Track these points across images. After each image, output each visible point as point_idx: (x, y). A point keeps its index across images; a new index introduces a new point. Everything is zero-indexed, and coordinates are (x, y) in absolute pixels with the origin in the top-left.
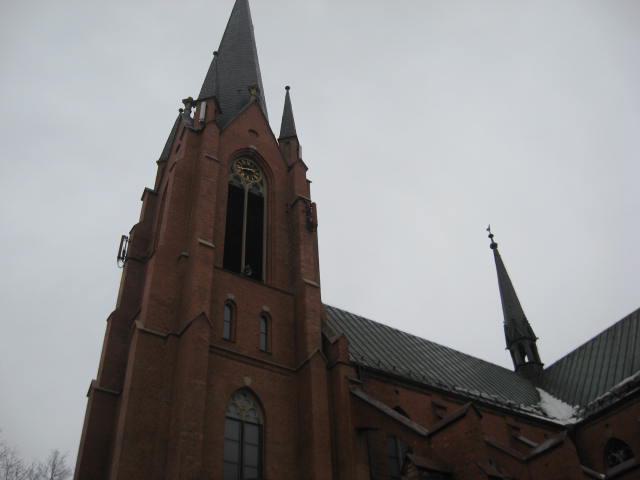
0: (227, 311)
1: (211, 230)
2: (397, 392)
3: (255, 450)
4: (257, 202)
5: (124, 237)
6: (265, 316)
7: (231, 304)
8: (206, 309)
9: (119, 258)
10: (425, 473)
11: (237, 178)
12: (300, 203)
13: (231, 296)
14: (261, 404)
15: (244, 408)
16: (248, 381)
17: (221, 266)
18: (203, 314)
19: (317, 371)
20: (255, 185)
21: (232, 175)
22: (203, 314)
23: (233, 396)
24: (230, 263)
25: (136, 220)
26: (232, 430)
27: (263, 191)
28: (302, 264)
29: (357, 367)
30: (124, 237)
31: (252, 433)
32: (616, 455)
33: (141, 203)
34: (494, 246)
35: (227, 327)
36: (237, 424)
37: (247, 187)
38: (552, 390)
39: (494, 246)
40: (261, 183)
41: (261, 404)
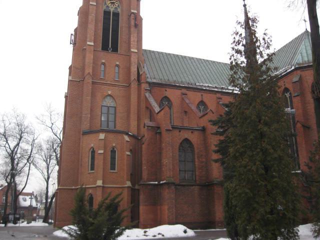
0: (103, 66)
1: (93, 37)
2: (166, 90)
3: (113, 116)
4: (116, 15)
5: (72, 34)
6: (117, 66)
7: (104, 64)
8: (91, 71)
9: (71, 43)
10: (150, 128)
11: (108, 7)
12: (132, 15)
13: (103, 61)
14: (114, 99)
15: (109, 102)
16: (110, 92)
17: (100, 49)
18: (89, 73)
19: (134, 85)
20: (116, 8)
21: (105, 6)
22: (89, 73)
23: (104, 98)
24: (105, 48)
25: (76, 25)
26: (105, 110)
27: (119, 10)
28: (132, 43)
29: (150, 84)
30: (72, 34)
31: (112, 111)
32: (286, 94)
33: (77, 17)
34: (245, 6)
35: (102, 73)
36: (106, 108)
37: (112, 10)
38: (194, 98)
39: (245, 6)
40: (119, 6)
41: (114, 99)
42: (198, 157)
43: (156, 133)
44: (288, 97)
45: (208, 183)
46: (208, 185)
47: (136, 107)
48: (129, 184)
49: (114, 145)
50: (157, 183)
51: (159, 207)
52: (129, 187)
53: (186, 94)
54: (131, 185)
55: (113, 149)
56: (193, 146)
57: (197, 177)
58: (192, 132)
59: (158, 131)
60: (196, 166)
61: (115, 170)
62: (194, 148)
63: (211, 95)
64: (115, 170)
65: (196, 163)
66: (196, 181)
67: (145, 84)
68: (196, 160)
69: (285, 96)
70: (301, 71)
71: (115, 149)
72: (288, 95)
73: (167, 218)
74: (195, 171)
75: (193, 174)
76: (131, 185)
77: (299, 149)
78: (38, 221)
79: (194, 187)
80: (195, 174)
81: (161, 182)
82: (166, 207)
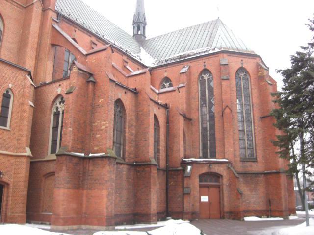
10: (81, 72)
29: (58, 14)
32: (204, 76)
42: (129, 128)
43: (88, 82)
44: (206, 79)
45: (136, 162)
46: (136, 165)
47: (36, 40)
48: (28, 152)
49: (10, 86)
50: (83, 155)
51: (85, 192)
52: (28, 157)
53: (96, 45)
54: (31, 155)
55: (7, 92)
56: (125, 110)
57: (126, 153)
58: (125, 93)
59: (92, 79)
60: (127, 138)
61: (6, 126)
62: (125, 114)
63: (118, 55)
64: (6, 126)
65: (127, 135)
66: (124, 158)
67: (54, 13)
68: (127, 130)
69: (203, 77)
70: (228, 56)
71: (10, 93)
72: (206, 77)
73: (105, 210)
74: (124, 146)
75: (120, 149)
76: (31, 155)
77: (225, 136)
78: (188, 188)
79: (122, 166)
80: (124, 149)
81: (91, 155)
82: (105, 193)
